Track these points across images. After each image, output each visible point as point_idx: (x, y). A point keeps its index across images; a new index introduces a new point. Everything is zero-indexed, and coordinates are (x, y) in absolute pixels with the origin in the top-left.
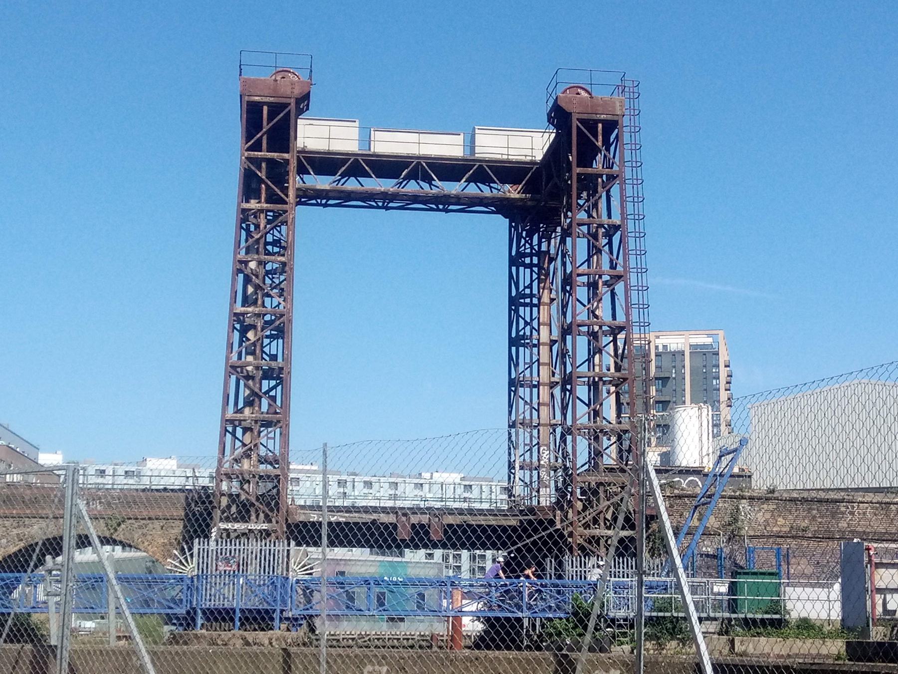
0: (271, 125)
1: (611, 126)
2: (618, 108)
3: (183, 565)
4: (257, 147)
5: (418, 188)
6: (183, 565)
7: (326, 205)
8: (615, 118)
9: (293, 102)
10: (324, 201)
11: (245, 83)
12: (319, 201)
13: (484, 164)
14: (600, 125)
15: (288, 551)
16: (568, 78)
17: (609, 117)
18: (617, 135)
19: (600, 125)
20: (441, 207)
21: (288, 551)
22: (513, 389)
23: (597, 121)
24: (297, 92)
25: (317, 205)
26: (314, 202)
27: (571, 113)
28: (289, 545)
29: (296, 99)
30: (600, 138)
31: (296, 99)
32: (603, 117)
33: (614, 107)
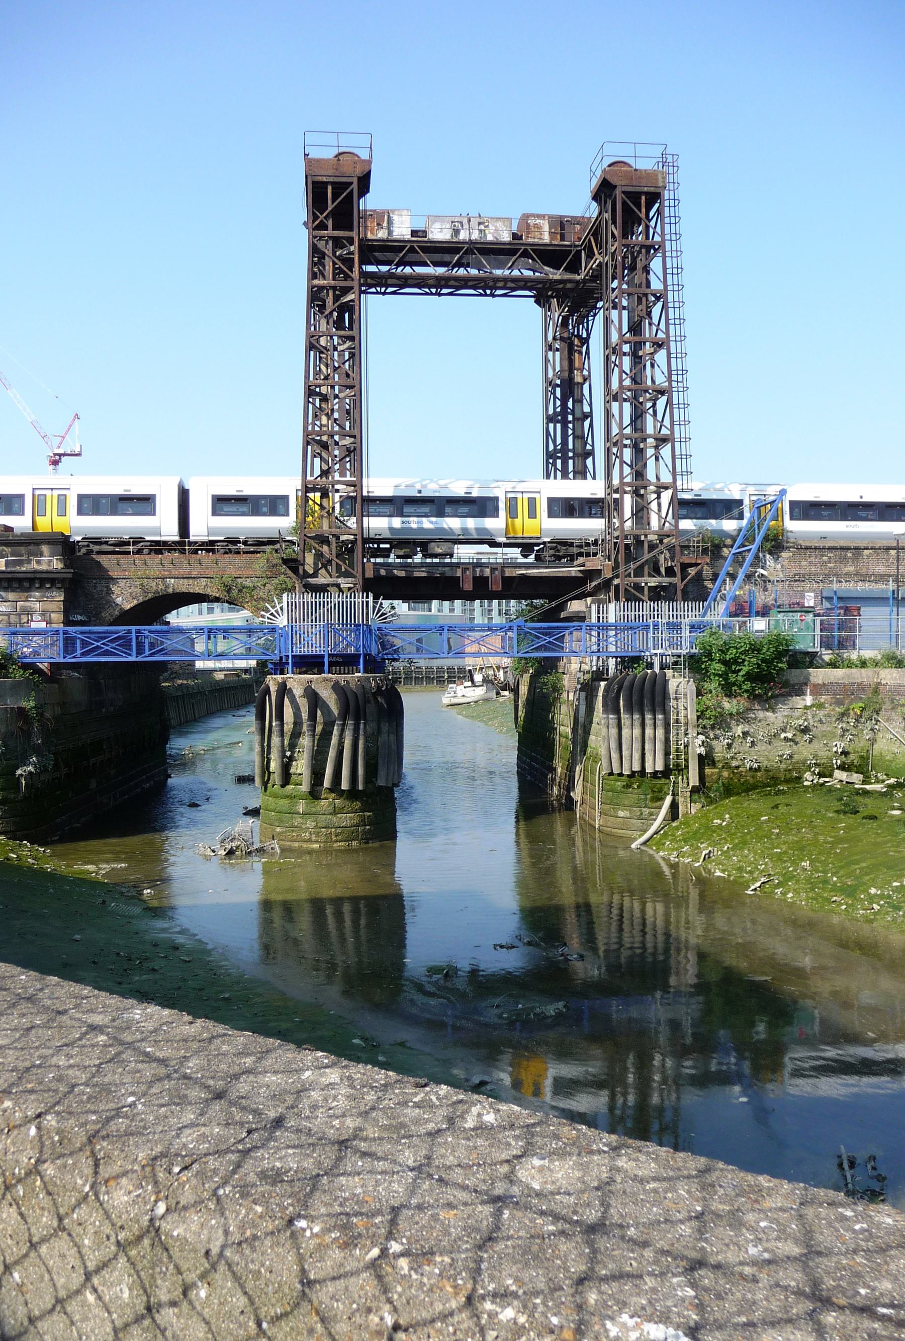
0: (335, 204)
1: (654, 197)
2: (660, 180)
3: (274, 616)
4: (322, 226)
5: (465, 272)
6: (274, 616)
7: (384, 293)
8: (657, 190)
9: (355, 181)
10: (383, 289)
11: (310, 163)
12: (379, 289)
13: (528, 248)
14: (643, 198)
15: (599, 613)
16: (615, 153)
17: (652, 190)
18: (658, 210)
19: (643, 198)
20: (488, 292)
21: (599, 613)
22: (551, 461)
23: (641, 193)
24: (359, 171)
25: (377, 293)
26: (373, 290)
27: (616, 186)
28: (367, 597)
29: (359, 178)
30: (643, 210)
31: (359, 178)
32: (646, 189)
33: (657, 180)
